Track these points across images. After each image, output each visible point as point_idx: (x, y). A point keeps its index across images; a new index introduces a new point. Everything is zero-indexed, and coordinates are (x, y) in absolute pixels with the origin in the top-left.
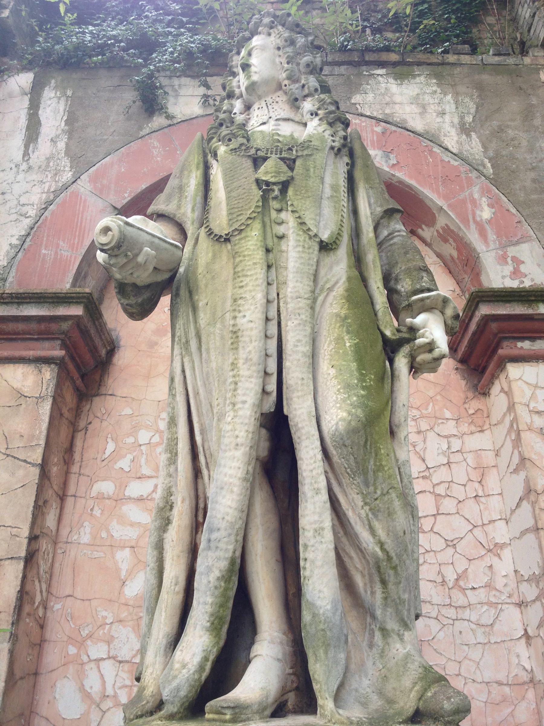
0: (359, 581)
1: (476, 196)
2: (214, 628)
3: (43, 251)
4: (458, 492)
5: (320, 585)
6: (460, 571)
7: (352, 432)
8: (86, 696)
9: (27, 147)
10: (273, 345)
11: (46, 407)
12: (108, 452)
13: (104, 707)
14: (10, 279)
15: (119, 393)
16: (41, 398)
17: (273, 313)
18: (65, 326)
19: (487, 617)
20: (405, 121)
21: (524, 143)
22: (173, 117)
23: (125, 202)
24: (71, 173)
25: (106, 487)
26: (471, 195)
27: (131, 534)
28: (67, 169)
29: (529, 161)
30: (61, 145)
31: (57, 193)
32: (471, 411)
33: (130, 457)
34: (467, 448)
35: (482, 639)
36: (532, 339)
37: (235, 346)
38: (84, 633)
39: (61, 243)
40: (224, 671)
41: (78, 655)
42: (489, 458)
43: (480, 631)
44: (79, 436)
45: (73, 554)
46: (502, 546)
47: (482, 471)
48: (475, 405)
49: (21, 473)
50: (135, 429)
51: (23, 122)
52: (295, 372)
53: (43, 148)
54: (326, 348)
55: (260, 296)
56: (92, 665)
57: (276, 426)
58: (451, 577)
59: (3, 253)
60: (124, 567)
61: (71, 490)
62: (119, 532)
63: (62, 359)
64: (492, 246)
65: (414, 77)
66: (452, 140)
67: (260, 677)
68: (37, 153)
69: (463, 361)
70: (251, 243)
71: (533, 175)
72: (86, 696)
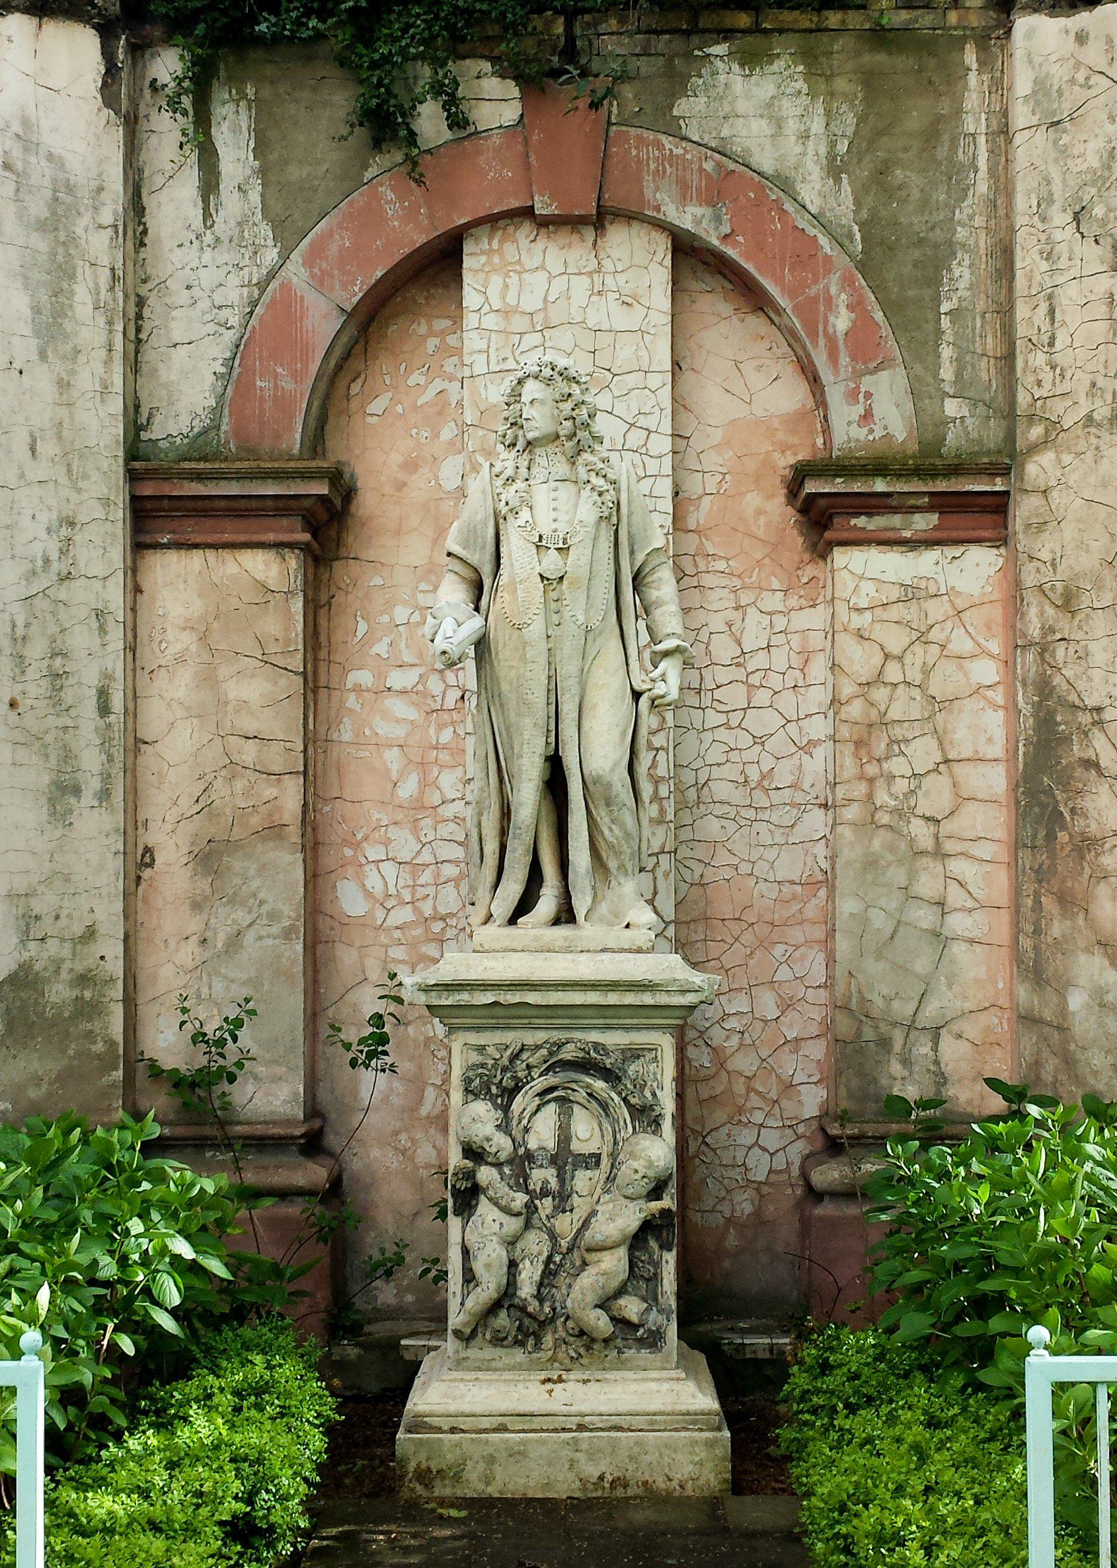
1: (833, 290)
3: (259, 383)
4: (775, 681)
6: (765, 771)
8: (369, 895)
12: (360, 634)
14: (224, 428)
15: (363, 555)
17: (553, 686)
18: (306, 503)
20: (747, 150)
21: (915, 194)
23: (355, 300)
24: (276, 250)
26: (827, 289)
27: (399, 732)
28: (270, 242)
29: (916, 228)
30: (255, 197)
31: (263, 286)
32: (805, 580)
34: (792, 628)
35: (779, 839)
36: (870, 515)
38: (359, 837)
39: (280, 370)
41: (355, 856)
44: (323, 612)
45: (335, 754)
47: (806, 656)
48: (809, 571)
49: (283, 682)
50: (389, 605)
53: (231, 205)
56: (372, 866)
57: (555, 763)
58: (754, 774)
60: (395, 767)
61: (323, 681)
63: (307, 544)
64: (843, 376)
65: (772, 58)
66: (813, 189)
68: (222, 213)
71: (916, 254)
72: (369, 895)
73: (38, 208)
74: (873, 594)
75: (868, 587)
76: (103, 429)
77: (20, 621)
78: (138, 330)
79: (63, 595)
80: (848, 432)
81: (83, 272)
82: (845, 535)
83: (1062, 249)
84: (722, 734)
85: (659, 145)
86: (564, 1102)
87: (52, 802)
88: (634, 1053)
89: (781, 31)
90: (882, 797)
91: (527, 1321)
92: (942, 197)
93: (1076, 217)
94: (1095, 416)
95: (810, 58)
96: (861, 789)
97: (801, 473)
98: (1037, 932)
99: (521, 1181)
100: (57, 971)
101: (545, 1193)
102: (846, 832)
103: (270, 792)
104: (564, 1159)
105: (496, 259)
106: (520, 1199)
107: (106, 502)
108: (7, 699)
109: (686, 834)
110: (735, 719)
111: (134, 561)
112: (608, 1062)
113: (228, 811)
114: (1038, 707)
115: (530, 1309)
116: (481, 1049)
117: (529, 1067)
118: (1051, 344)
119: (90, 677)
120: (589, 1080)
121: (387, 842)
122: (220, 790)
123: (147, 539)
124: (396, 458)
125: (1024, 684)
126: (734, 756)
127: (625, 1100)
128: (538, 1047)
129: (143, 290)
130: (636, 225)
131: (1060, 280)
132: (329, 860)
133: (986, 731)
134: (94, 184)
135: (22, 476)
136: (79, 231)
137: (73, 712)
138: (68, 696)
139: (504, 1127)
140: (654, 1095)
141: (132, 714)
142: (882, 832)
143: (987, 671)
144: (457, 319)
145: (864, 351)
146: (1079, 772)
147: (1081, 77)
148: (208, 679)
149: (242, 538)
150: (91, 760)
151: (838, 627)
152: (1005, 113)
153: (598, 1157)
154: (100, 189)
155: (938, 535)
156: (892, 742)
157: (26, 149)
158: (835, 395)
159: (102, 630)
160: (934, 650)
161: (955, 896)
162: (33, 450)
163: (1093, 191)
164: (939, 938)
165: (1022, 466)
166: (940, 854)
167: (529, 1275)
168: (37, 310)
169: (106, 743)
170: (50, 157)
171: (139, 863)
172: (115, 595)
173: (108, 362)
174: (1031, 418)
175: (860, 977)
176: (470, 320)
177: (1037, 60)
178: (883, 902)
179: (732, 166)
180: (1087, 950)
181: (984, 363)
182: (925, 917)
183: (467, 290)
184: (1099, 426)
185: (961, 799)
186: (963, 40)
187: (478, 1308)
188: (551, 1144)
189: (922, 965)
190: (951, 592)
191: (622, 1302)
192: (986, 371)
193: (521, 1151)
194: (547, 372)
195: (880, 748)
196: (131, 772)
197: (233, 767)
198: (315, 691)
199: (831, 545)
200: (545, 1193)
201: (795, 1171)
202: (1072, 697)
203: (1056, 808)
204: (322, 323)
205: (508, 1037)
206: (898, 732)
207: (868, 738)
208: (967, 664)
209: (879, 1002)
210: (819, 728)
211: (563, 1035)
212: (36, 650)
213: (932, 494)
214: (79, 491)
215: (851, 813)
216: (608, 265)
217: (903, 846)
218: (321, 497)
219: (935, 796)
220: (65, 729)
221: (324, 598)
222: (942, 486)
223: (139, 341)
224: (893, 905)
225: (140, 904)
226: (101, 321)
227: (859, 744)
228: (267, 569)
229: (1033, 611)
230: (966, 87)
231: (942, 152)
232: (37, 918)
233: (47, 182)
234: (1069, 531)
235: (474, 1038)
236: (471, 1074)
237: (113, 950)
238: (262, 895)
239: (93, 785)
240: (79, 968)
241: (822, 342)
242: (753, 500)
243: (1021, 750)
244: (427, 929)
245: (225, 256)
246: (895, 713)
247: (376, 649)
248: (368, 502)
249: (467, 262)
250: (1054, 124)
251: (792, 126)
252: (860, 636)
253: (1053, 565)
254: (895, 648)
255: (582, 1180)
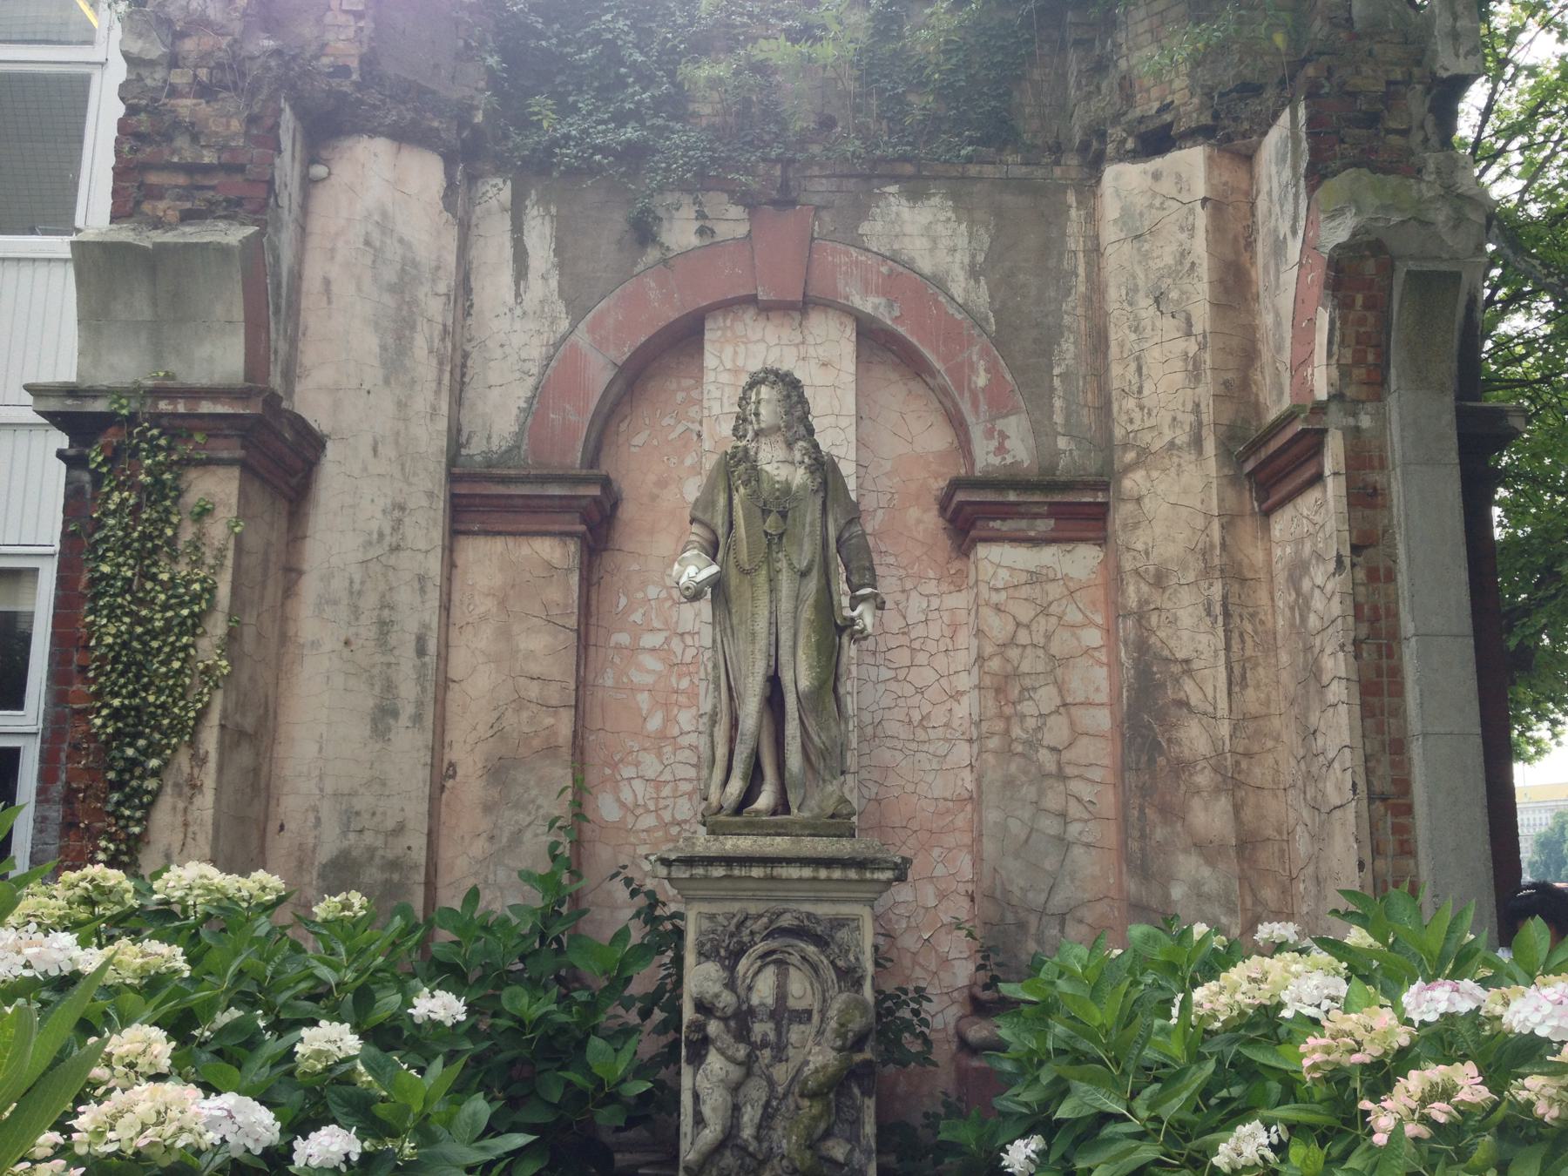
0: (813, 758)
1: (975, 358)
2: (744, 778)
4: (931, 646)
5: (794, 761)
7: (812, 693)
8: (623, 805)
9: (517, 284)
10: (773, 638)
11: (575, 579)
13: (638, 812)
14: (524, 447)
16: (569, 570)
18: (584, 503)
19: (943, 750)
20: (912, 259)
22: (668, 249)
25: (623, 638)
27: (649, 679)
30: (554, 283)
31: (556, 346)
33: (641, 611)
34: (944, 607)
36: (1004, 519)
37: (753, 642)
40: (749, 796)
42: (962, 616)
43: (935, 760)
44: (594, 590)
46: (963, 693)
47: (955, 627)
48: (957, 565)
49: (561, 637)
50: (644, 585)
51: (508, 252)
52: (785, 656)
54: (801, 642)
55: (766, 613)
57: (774, 683)
58: (916, 716)
59: (513, 418)
60: (645, 707)
61: (592, 641)
62: (638, 678)
63: (584, 534)
66: (959, 286)
67: (765, 800)
69: (951, 521)
70: (762, 578)
73: (389, 275)
74: (1007, 577)
75: (1004, 574)
76: (430, 439)
77: (357, 578)
78: (463, 375)
79: (392, 561)
80: (985, 457)
81: (422, 325)
82: (984, 534)
83: (1147, 323)
84: (893, 686)
85: (848, 254)
86: (782, 964)
87: (374, 721)
88: (839, 923)
89: (935, 178)
90: (1017, 731)
91: (748, 1160)
92: (1053, 294)
93: (1157, 301)
94: (1177, 441)
95: (955, 196)
96: (999, 726)
97: (956, 485)
98: (1143, 836)
99: (742, 1034)
100: (372, 858)
101: (765, 1044)
102: (990, 759)
103: (549, 721)
104: (782, 1014)
105: (729, 334)
106: (742, 1052)
107: (430, 495)
108: (343, 639)
109: (865, 761)
110: (902, 674)
111: (452, 544)
112: (819, 930)
113: (515, 735)
114: (1137, 662)
115: (751, 1149)
116: (712, 917)
117: (752, 933)
118: (1140, 391)
119: (412, 626)
120: (802, 945)
121: (637, 764)
122: (510, 719)
123: (462, 527)
124: (652, 478)
125: (1126, 644)
126: (901, 702)
127: (832, 962)
128: (761, 916)
129: (468, 347)
130: (831, 312)
131: (1146, 345)
132: (592, 777)
133: (1095, 682)
134: (433, 264)
135: (365, 469)
136: (421, 296)
137: (396, 652)
138: (393, 640)
139: (730, 985)
140: (857, 959)
141: (443, 656)
142: (1018, 759)
143: (1093, 637)
144: (699, 381)
145: (999, 404)
146: (1173, 710)
147: (1157, 202)
148: (505, 633)
149: (535, 528)
150: (408, 690)
151: (981, 602)
152: (1097, 237)
153: (809, 1013)
154: (438, 268)
155: (1054, 534)
156: (1024, 689)
157: (383, 233)
158: (977, 433)
159: (423, 590)
160: (1054, 620)
161: (1074, 810)
162: (375, 451)
163: (1169, 281)
164: (1063, 843)
165: (1119, 481)
166: (1061, 776)
167: (750, 1116)
168: (384, 348)
169: (421, 678)
170: (401, 241)
171: (441, 775)
172: (434, 565)
173: (437, 392)
174: (1125, 447)
175: (1003, 873)
176: (709, 377)
177: (1123, 194)
178: (1019, 813)
179: (901, 269)
180: (1186, 851)
181: (1085, 411)
182: (1050, 826)
183: (707, 355)
184: (1180, 448)
185: (1076, 734)
186: (1066, 187)
187: (705, 1149)
188: (770, 1001)
189: (1050, 864)
190: (1066, 577)
191: (830, 1143)
192: (1087, 418)
193: (745, 1007)
194: (772, 378)
195: (1014, 693)
196: (440, 702)
197: (520, 702)
198: (586, 647)
199: (975, 542)
200: (765, 1044)
201: (951, 1030)
202: (1166, 653)
203: (1155, 738)
204: (599, 375)
205: (735, 907)
206: (1028, 682)
207: (1004, 687)
208: (1078, 631)
209: (1018, 893)
210: (964, 682)
211: (781, 906)
212: (370, 601)
213: (1050, 504)
214: (410, 484)
215: (993, 743)
216: (810, 340)
217: (1033, 770)
218: (594, 498)
219: (1057, 731)
220: (389, 665)
221: (595, 579)
222: (1058, 498)
223: (463, 383)
224: (1027, 815)
225: (443, 808)
226: (434, 362)
227: (998, 691)
228: (552, 552)
229: (1131, 589)
230: (1068, 219)
231: (1052, 263)
232: (358, 814)
233: (398, 258)
234: (1159, 529)
235: (706, 908)
236: (703, 939)
237: (418, 842)
238: (539, 802)
239: (407, 710)
240: (390, 855)
241: (967, 394)
242: (914, 513)
243: (1125, 694)
244: (667, 832)
245: (532, 325)
246: (1025, 667)
247: (632, 618)
248: (628, 511)
249: (708, 336)
250: (1137, 237)
251: (944, 243)
252: (998, 608)
253: (1147, 553)
254: (1024, 619)
255: (795, 1033)
